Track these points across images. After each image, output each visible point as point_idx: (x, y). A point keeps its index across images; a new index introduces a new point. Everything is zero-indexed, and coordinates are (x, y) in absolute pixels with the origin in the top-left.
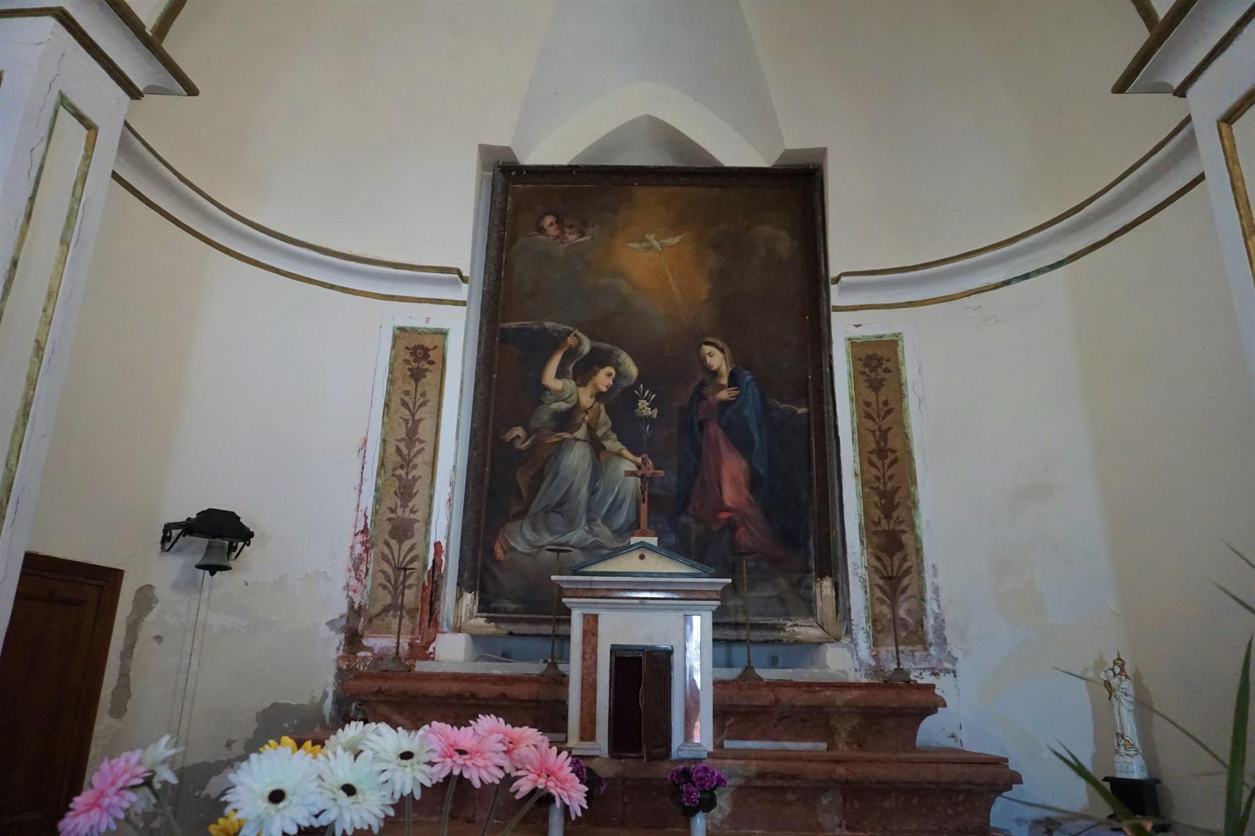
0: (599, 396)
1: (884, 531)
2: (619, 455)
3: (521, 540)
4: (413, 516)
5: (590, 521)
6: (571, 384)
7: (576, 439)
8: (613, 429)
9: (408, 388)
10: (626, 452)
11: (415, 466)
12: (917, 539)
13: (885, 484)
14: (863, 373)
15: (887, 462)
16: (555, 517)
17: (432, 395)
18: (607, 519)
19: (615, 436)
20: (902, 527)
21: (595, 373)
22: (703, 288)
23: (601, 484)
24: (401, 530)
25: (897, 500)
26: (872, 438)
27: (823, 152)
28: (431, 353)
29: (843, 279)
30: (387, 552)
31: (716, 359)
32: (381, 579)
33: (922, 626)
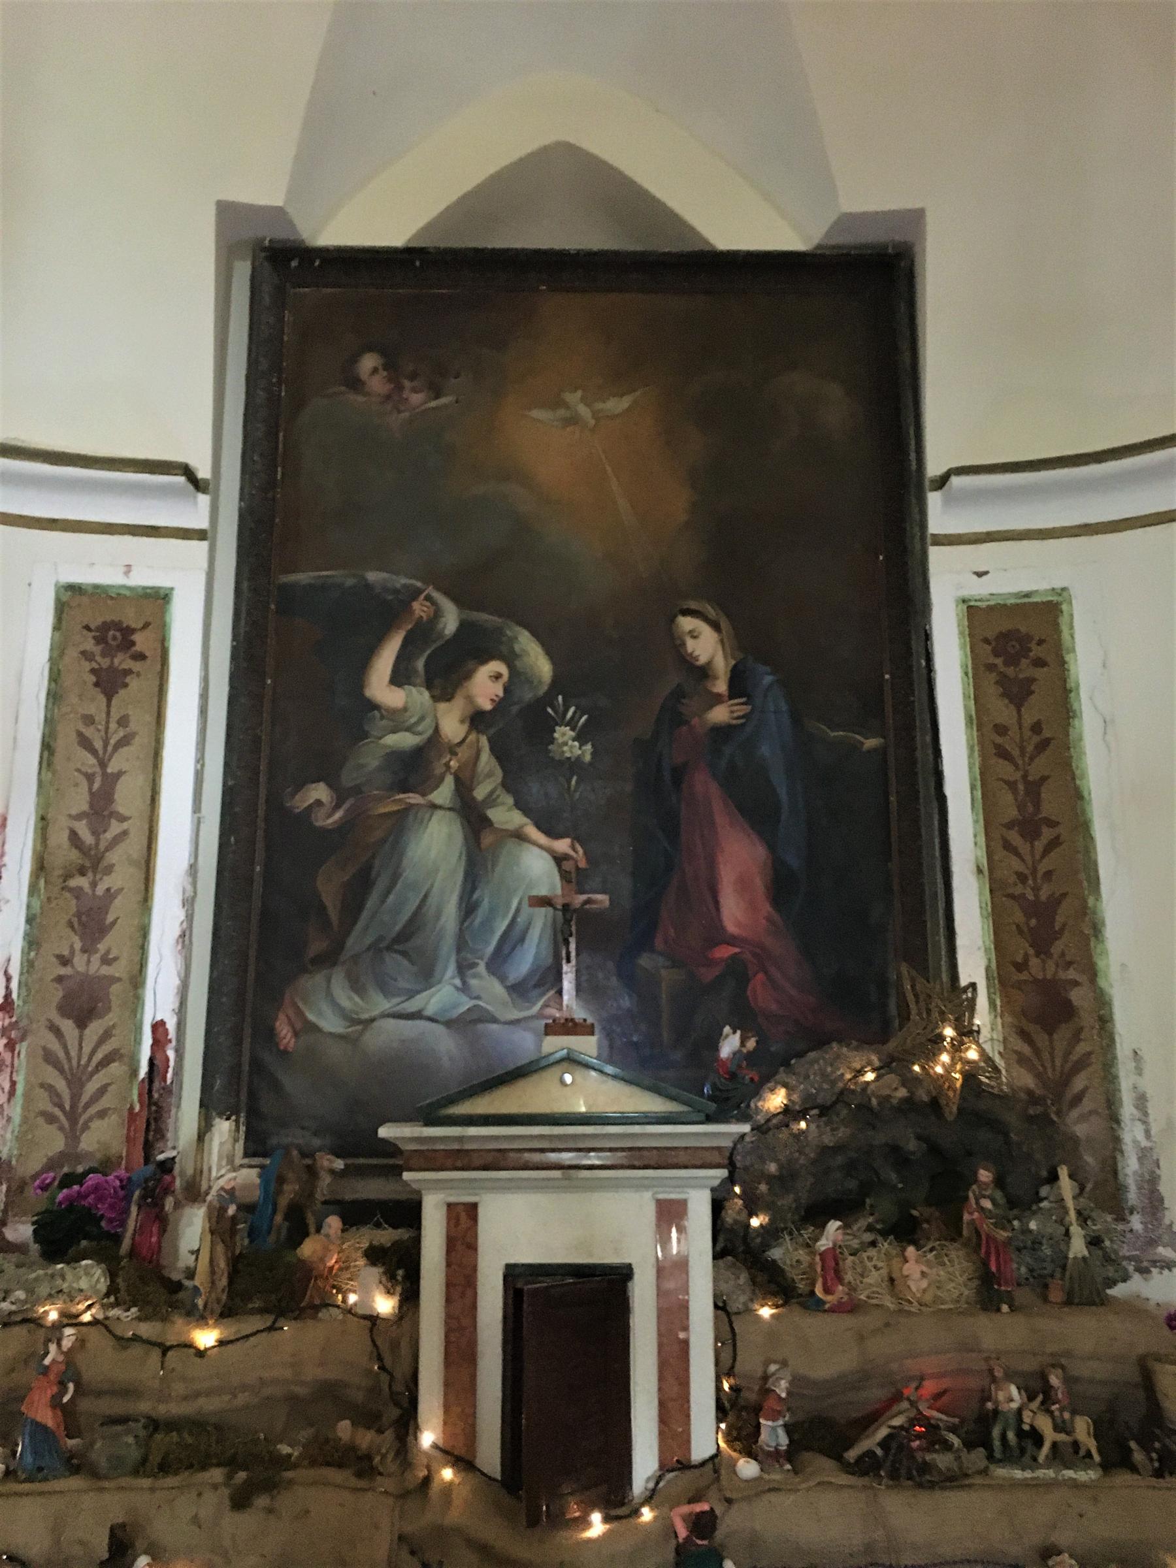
0: (477, 720)
1: (1036, 981)
2: (519, 836)
3: (327, 1007)
4: (105, 970)
5: (463, 969)
6: (420, 696)
7: (434, 807)
8: (506, 785)
9: (91, 709)
10: (532, 832)
11: (109, 870)
12: (1102, 1002)
13: (1036, 890)
14: (991, 667)
15: (1039, 845)
16: (393, 961)
17: (140, 721)
18: (498, 963)
19: (510, 800)
20: (1072, 974)
21: (468, 675)
22: (677, 503)
23: (485, 896)
24: (84, 1003)
25: (1059, 920)
26: (1009, 797)
27: (917, 217)
28: (137, 637)
29: (955, 481)
30: (55, 1046)
31: (705, 643)
32: (44, 1102)
33: (1115, 1173)
